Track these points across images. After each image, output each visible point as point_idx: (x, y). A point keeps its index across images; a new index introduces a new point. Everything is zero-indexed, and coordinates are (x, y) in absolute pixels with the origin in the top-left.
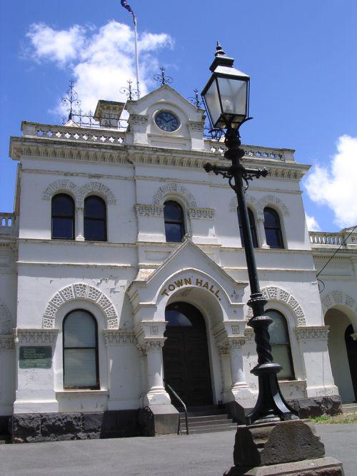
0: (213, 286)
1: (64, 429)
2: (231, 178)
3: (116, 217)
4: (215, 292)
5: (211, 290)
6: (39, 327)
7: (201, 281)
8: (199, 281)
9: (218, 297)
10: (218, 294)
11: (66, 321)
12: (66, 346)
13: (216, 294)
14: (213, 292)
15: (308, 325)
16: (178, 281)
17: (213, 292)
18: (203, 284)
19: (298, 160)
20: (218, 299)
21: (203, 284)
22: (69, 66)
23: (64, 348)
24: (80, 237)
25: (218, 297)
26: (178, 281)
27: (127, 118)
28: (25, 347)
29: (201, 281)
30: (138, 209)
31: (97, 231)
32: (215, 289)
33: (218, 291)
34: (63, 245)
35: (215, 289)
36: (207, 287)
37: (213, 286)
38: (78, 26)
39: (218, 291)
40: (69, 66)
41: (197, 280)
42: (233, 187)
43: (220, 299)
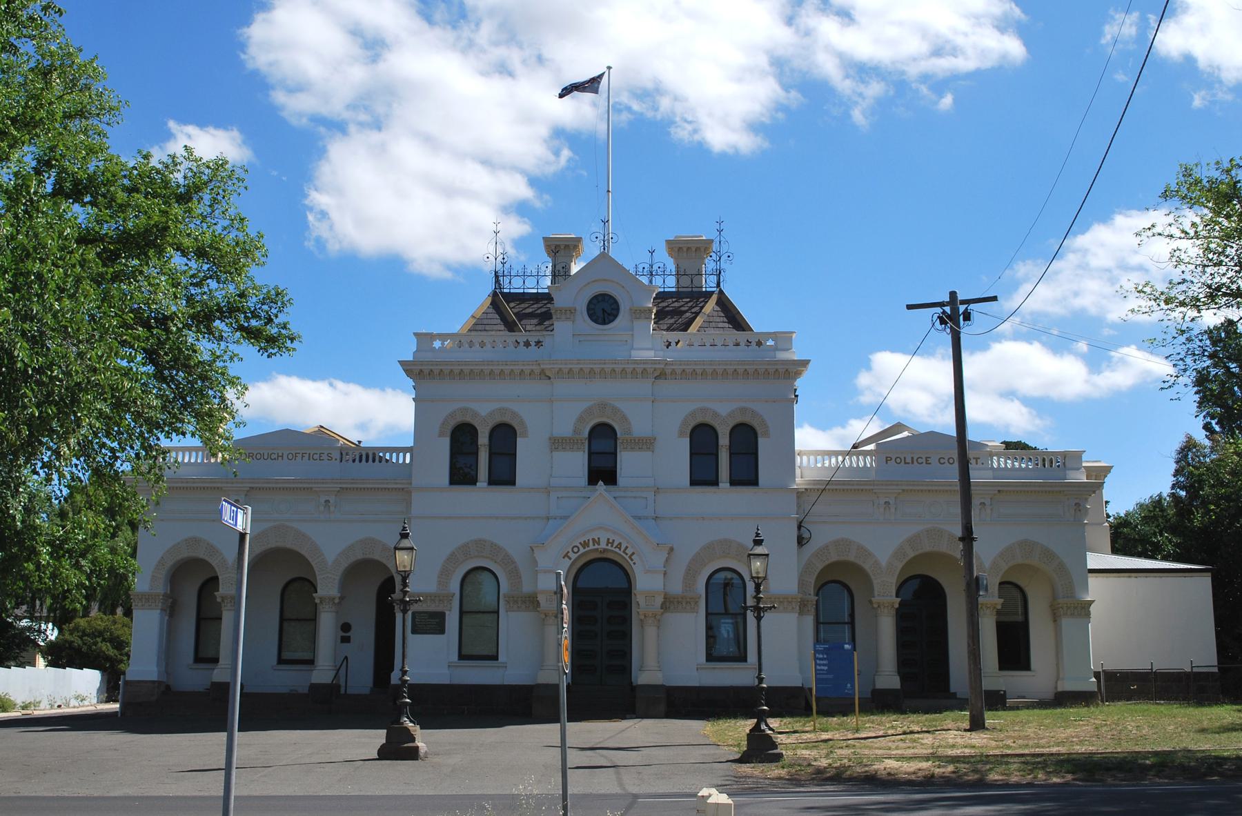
0: (627, 547)
2: (400, 605)
3: (528, 454)
4: (629, 554)
5: (624, 552)
6: (689, 439)
7: (614, 541)
8: (611, 541)
9: (632, 560)
10: (633, 557)
11: (465, 587)
12: (496, 615)
13: (630, 557)
14: (627, 554)
16: (585, 541)
17: (627, 554)
18: (615, 544)
19: (796, 354)
20: (631, 563)
21: (615, 544)
23: (708, 614)
24: (482, 482)
25: (632, 560)
26: (585, 541)
28: (417, 612)
29: (614, 541)
30: (558, 443)
31: (504, 476)
32: (629, 551)
33: (633, 554)
34: (463, 492)
35: (629, 551)
36: (620, 550)
37: (627, 547)
39: (633, 554)
41: (608, 539)
42: (402, 610)
43: (634, 563)
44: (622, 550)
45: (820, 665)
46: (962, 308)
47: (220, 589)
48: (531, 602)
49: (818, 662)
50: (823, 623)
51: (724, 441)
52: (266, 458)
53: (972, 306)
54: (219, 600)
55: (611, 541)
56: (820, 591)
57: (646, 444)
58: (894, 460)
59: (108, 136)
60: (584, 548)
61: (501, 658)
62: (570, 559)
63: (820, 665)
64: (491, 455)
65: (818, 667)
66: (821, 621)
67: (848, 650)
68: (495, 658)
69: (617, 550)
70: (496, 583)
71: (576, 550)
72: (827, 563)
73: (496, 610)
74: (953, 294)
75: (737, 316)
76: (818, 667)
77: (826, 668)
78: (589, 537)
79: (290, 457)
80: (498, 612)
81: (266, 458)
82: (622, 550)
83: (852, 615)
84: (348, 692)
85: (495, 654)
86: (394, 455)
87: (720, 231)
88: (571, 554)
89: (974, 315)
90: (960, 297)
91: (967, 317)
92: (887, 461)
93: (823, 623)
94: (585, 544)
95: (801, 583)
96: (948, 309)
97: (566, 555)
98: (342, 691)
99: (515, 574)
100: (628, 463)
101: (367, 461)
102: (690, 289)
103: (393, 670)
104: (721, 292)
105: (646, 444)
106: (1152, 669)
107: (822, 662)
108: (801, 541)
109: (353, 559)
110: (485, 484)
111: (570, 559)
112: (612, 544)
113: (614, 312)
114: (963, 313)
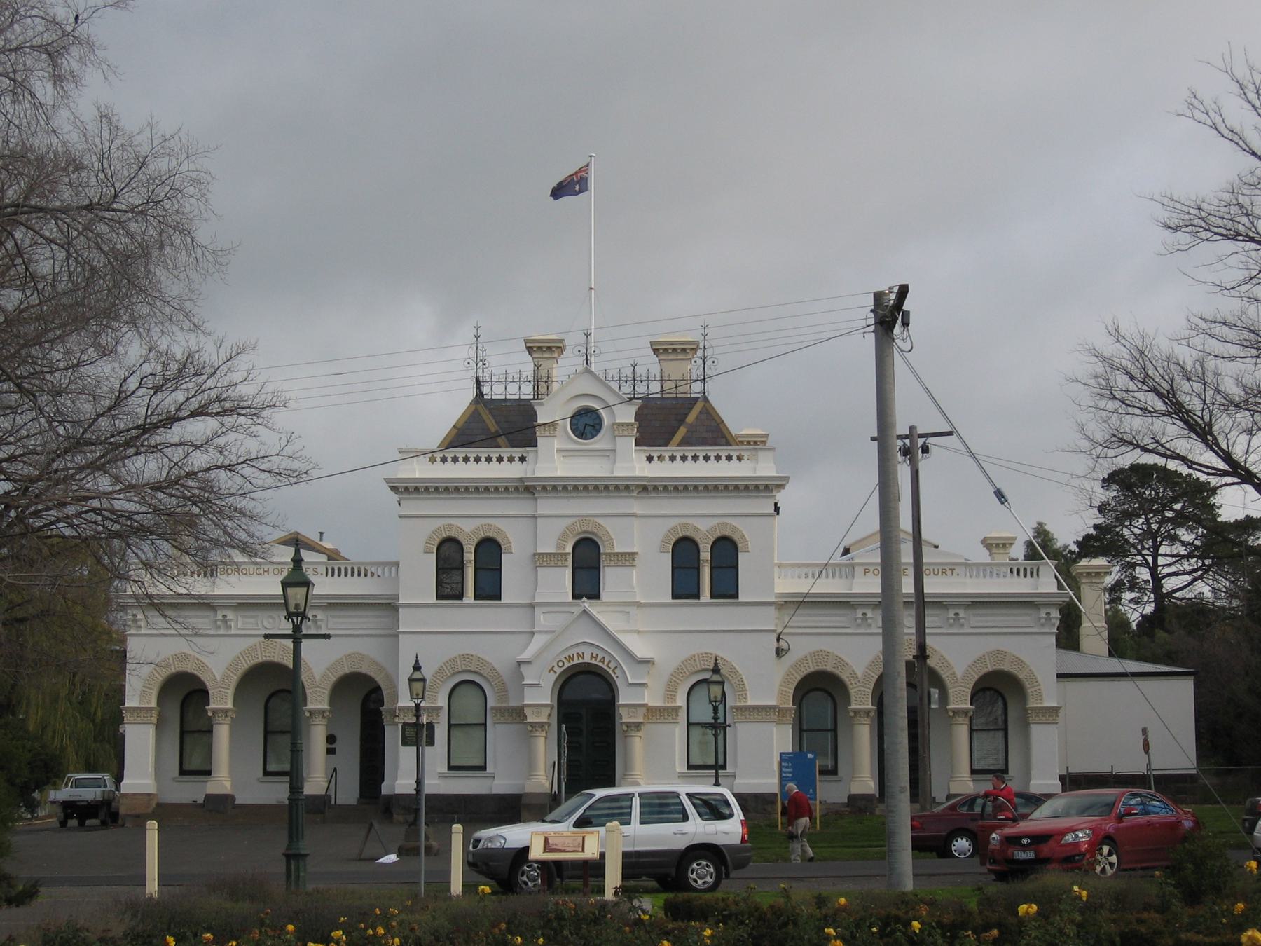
0: (610, 661)
1: (371, 932)
5: (608, 665)
8: (594, 655)
9: (615, 673)
13: (613, 671)
15: (616, 551)
18: (599, 659)
21: (599, 659)
22: (999, 802)
25: (615, 673)
26: (569, 656)
27: (1168, 467)
30: (540, 559)
31: (489, 590)
32: (612, 665)
33: (616, 667)
36: (603, 663)
37: (610, 661)
38: (746, 830)
39: (616, 667)
40: (999, 802)
44: (606, 663)
45: (785, 772)
46: (921, 441)
47: (211, 703)
48: (518, 714)
49: (783, 769)
50: (806, 731)
51: (705, 555)
52: (251, 572)
53: (931, 440)
54: (210, 714)
55: (594, 655)
56: (804, 701)
57: (628, 559)
58: (871, 571)
59: (320, 466)
60: (569, 662)
61: (490, 769)
62: (555, 672)
63: (785, 772)
64: (476, 569)
65: (784, 775)
66: (829, 734)
67: (810, 759)
68: (484, 768)
69: (601, 664)
70: (484, 697)
71: (561, 664)
72: (806, 672)
73: (975, 735)
74: (912, 428)
75: (721, 426)
76: (784, 775)
77: (790, 775)
78: (574, 651)
79: (276, 571)
80: (485, 725)
81: (251, 572)
82: (606, 663)
83: (1006, 721)
84: (338, 803)
85: (483, 764)
86: (379, 569)
87: (705, 336)
88: (556, 669)
89: (932, 448)
90: (920, 431)
91: (925, 450)
92: (865, 573)
93: (806, 731)
94: (570, 658)
95: (782, 694)
96: (907, 442)
97: (552, 669)
98: (333, 802)
99: (502, 691)
100: (611, 578)
101: (352, 575)
102: (674, 396)
103: (383, 781)
104: (706, 399)
105: (628, 559)
106: (1112, 772)
107: (787, 770)
108: (779, 653)
109: (340, 673)
110: (472, 601)
111: (555, 672)
112: (596, 658)
113: (597, 421)
114: (922, 447)
